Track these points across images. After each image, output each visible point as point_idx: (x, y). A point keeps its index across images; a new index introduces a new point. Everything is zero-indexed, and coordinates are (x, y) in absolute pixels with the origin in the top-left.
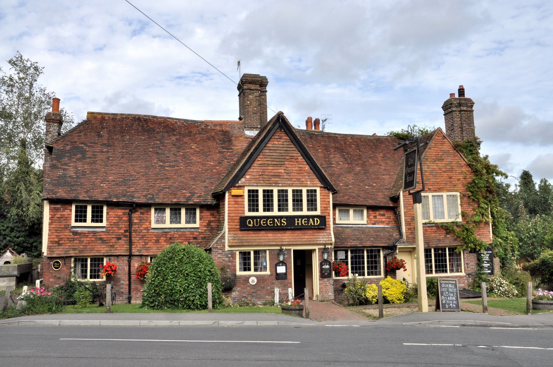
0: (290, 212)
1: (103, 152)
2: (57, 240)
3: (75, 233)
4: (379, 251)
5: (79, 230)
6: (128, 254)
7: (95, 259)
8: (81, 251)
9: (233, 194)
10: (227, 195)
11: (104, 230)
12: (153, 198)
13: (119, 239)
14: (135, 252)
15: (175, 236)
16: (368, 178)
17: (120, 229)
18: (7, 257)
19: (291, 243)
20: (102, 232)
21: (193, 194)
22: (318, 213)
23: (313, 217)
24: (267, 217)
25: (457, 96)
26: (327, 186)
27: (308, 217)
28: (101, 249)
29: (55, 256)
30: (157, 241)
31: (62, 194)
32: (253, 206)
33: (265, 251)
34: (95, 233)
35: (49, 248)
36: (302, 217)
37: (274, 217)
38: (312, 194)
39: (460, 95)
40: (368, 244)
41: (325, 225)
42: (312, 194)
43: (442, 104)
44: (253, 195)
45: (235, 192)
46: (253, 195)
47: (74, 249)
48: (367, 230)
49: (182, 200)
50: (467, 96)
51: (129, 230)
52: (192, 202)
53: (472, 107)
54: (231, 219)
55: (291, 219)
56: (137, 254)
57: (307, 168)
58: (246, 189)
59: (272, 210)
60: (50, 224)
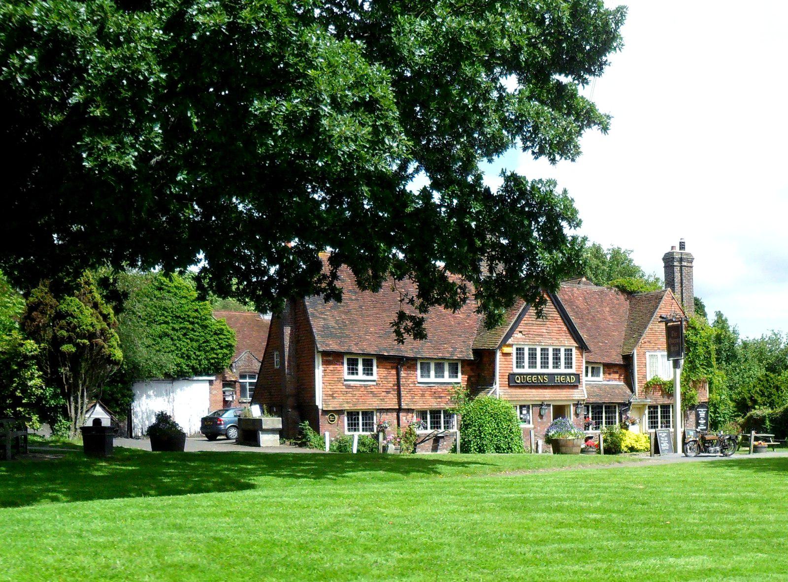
0: (551, 370)
1: (352, 300)
2: (331, 393)
3: (348, 387)
4: (615, 407)
5: (352, 383)
6: (397, 407)
7: (352, 412)
8: (354, 405)
9: (505, 352)
10: (499, 355)
11: (374, 383)
12: (419, 352)
13: (388, 392)
14: (404, 406)
15: (439, 390)
16: (599, 335)
17: (388, 382)
18: (98, 413)
19: (552, 399)
20: (374, 385)
21: (455, 349)
22: (573, 371)
23: (570, 375)
24: (532, 374)
25: (677, 249)
26: (582, 347)
27: (565, 374)
28: (372, 403)
29: (330, 409)
30: (423, 395)
31: (334, 346)
32: (519, 364)
33: (570, 405)
34: (366, 386)
35: (324, 401)
36: (561, 374)
37: (538, 374)
38: (569, 352)
39: (680, 249)
40: (607, 400)
41: (579, 382)
42: (569, 352)
43: (663, 256)
44: (520, 351)
45: (506, 350)
46: (520, 351)
47: (348, 403)
48: (603, 387)
49: (447, 355)
50: (687, 250)
51: (398, 385)
52: (456, 358)
53: (691, 262)
54: (502, 376)
55: (551, 376)
56: (406, 407)
57: (565, 328)
58: (515, 347)
59: (536, 367)
60: (324, 377)
